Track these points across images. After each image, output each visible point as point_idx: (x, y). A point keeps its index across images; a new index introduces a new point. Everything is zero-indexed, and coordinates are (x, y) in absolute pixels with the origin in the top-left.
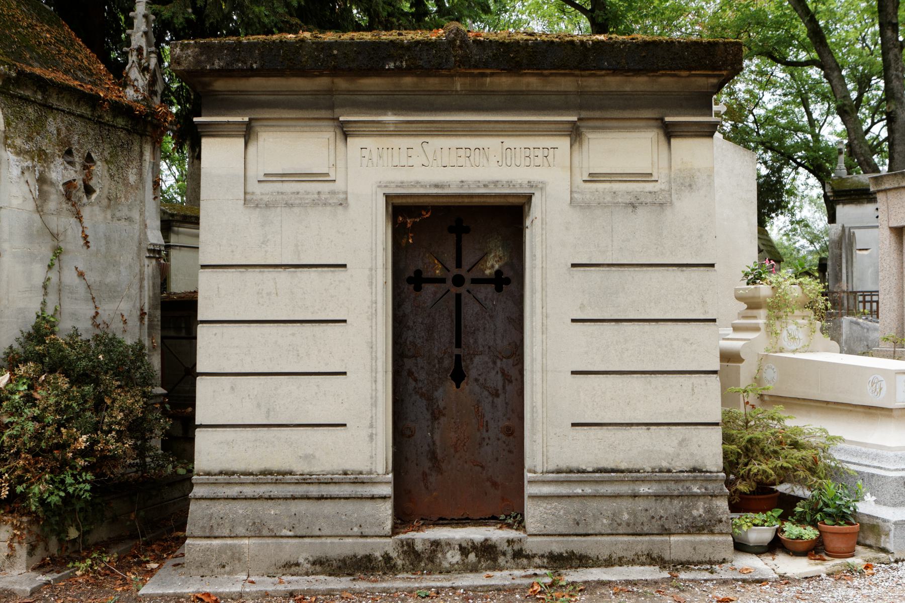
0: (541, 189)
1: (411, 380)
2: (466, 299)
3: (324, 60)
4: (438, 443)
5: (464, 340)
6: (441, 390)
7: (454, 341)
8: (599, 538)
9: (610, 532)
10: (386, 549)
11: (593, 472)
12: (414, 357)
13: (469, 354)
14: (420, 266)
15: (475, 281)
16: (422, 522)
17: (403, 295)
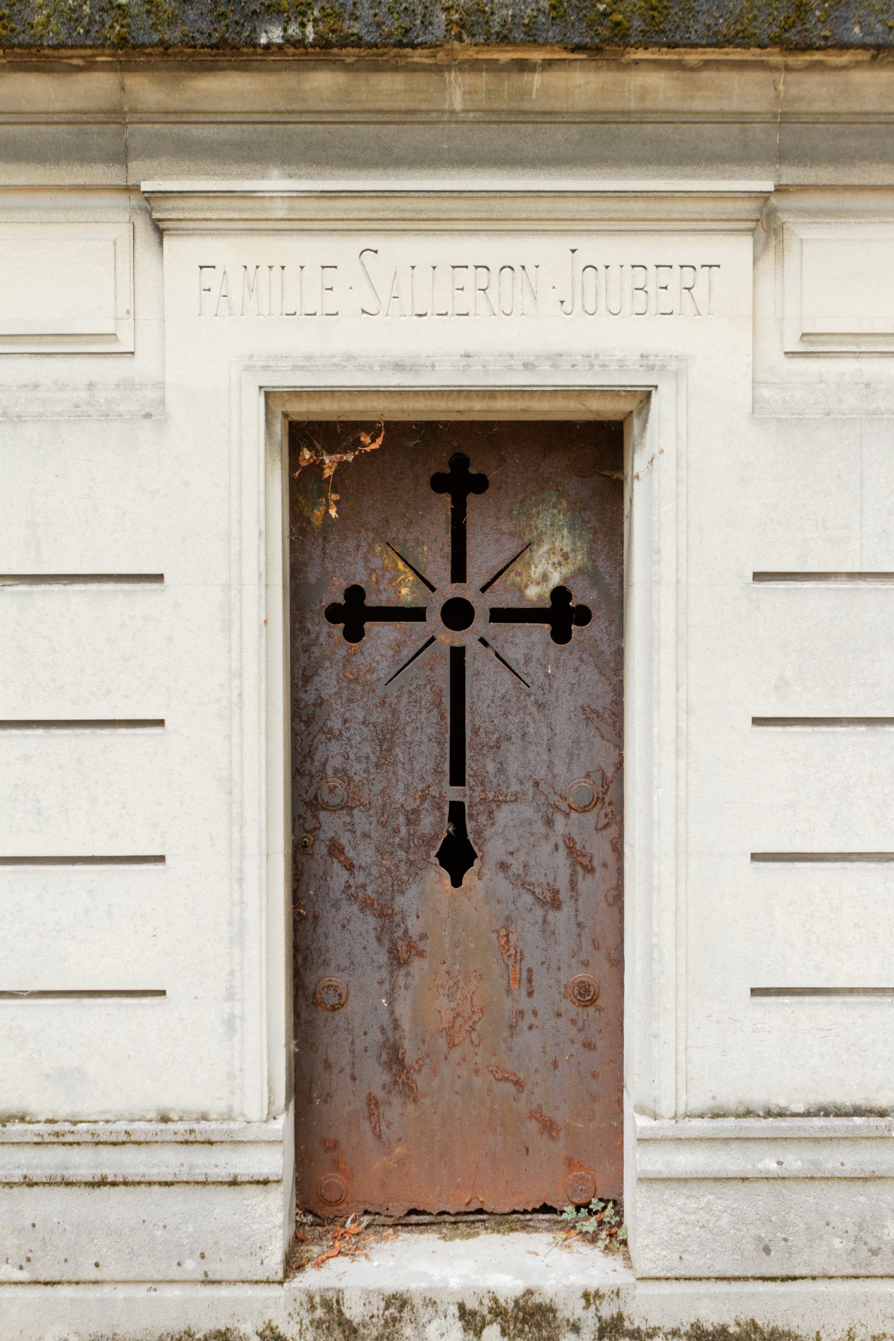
0: (677, 374)
1: (337, 867)
2: (477, 662)
3: (92, 22)
4: (406, 1024)
5: (470, 765)
6: (413, 891)
7: (447, 767)
8: (821, 1286)
9: (850, 1271)
10: (270, 1314)
11: (808, 1114)
12: (346, 807)
13: (484, 800)
14: (360, 578)
15: (499, 615)
16: (366, 1220)
17: (316, 651)
